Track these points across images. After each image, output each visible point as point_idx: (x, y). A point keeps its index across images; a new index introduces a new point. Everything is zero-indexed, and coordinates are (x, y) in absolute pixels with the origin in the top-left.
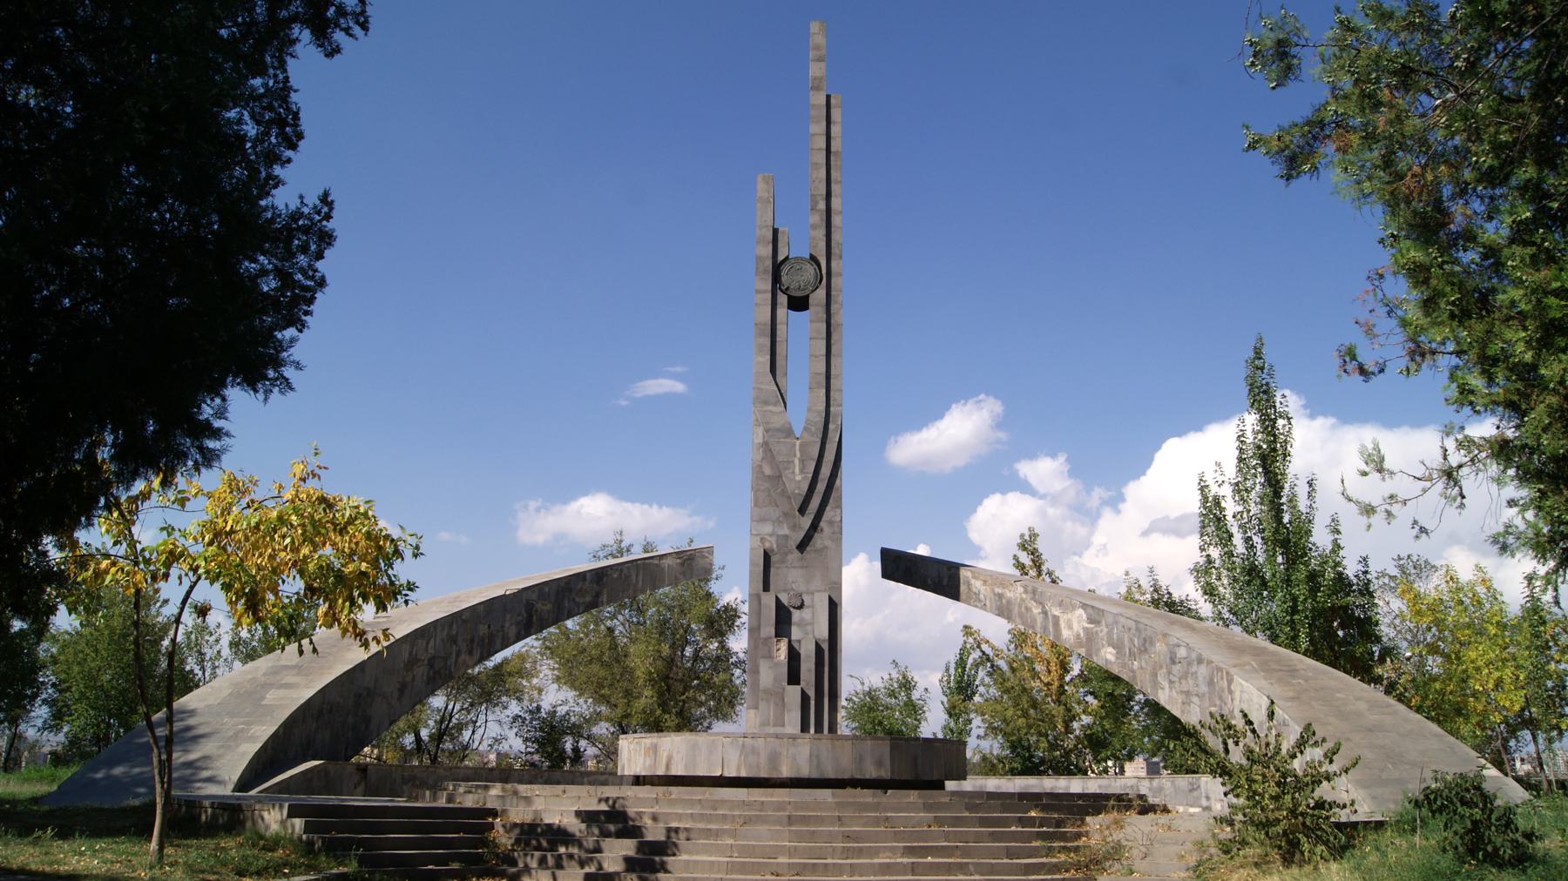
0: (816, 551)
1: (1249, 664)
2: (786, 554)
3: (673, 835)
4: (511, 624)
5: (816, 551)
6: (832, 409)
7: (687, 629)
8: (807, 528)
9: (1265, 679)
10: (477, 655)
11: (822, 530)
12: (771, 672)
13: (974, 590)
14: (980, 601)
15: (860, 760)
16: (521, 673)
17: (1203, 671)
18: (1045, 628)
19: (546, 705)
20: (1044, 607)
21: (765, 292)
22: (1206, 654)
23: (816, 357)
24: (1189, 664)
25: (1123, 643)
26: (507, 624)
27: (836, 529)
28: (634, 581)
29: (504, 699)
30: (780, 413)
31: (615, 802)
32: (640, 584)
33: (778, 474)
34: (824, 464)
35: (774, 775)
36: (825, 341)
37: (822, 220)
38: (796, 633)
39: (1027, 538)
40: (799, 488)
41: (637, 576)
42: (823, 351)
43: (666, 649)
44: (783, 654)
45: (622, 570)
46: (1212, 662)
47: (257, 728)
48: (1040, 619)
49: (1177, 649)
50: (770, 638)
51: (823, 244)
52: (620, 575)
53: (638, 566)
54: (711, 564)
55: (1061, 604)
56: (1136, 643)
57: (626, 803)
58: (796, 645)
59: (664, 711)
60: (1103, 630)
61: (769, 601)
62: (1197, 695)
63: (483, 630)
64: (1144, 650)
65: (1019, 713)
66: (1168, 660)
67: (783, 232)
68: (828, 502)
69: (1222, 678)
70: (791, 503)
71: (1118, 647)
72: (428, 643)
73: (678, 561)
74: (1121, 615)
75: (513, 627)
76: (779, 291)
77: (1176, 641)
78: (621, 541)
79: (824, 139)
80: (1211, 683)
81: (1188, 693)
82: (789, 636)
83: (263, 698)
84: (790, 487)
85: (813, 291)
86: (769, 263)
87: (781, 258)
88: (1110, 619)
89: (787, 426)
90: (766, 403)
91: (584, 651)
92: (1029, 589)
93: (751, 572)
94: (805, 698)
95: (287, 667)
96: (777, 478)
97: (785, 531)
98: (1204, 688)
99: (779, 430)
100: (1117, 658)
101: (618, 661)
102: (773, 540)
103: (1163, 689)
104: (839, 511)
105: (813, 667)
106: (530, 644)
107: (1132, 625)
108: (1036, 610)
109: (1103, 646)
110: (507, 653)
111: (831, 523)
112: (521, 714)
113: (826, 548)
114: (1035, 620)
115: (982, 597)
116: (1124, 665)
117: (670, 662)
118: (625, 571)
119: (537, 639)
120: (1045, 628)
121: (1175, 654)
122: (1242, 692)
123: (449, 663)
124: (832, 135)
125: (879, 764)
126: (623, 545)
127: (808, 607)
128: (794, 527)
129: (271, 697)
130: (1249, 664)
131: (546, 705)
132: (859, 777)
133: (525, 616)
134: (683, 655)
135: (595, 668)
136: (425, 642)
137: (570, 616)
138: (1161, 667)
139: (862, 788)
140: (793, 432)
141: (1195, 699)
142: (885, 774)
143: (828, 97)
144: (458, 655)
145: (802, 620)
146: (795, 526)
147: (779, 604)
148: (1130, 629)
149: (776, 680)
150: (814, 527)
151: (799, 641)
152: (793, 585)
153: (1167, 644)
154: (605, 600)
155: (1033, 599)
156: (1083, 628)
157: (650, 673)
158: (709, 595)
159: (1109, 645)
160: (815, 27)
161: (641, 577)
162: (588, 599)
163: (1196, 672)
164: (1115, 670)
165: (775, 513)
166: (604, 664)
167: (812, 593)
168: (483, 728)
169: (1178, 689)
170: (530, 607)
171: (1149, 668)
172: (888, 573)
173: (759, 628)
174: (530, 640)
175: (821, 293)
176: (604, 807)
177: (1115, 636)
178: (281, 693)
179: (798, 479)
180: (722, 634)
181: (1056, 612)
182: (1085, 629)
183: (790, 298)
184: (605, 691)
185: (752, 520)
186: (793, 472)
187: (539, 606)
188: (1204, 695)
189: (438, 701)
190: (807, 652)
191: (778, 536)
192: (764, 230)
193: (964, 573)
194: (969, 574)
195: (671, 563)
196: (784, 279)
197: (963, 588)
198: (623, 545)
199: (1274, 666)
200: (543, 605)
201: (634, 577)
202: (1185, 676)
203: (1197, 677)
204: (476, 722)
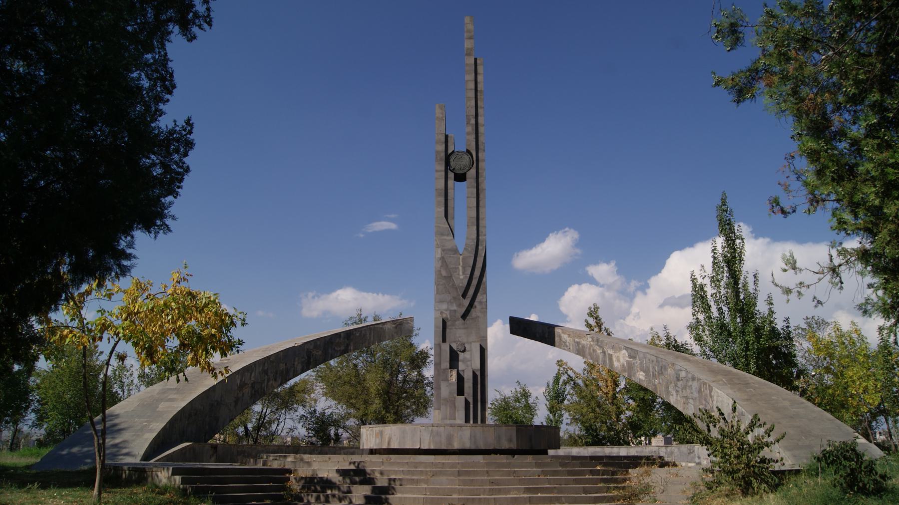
1: (722, 380)
2: (455, 321)
3: (392, 482)
6: (480, 238)
7: (399, 365)
9: (731, 389)
10: (279, 381)
11: (475, 307)
12: (448, 388)
13: (563, 340)
14: (567, 346)
17: (695, 384)
18: (604, 361)
19: (319, 409)
21: (441, 171)
22: (697, 375)
24: (687, 381)
25: (649, 369)
26: (296, 363)
27: (484, 307)
29: (295, 406)
30: (451, 240)
31: (359, 464)
32: (372, 339)
34: (476, 269)
35: (450, 448)
36: (476, 199)
38: (461, 366)
39: (593, 309)
40: (462, 283)
43: (387, 376)
45: (361, 331)
48: (601, 356)
49: (680, 372)
50: (447, 369)
51: (474, 144)
52: (360, 334)
53: (370, 329)
54: (413, 327)
55: (613, 347)
56: (657, 369)
57: (365, 465)
59: (387, 412)
60: (637, 362)
61: (446, 348)
62: (692, 399)
63: (282, 366)
65: (590, 410)
66: (675, 379)
67: (451, 137)
69: (706, 389)
71: (646, 371)
73: (394, 326)
74: (647, 353)
75: (300, 365)
77: (679, 368)
80: (700, 391)
81: (686, 398)
82: (457, 367)
83: (158, 407)
84: (457, 282)
85: (468, 170)
86: (443, 154)
87: (450, 151)
88: (641, 355)
90: (442, 234)
91: (340, 378)
94: (467, 403)
95: (171, 389)
96: (449, 278)
97: (454, 307)
98: (696, 395)
99: (450, 250)
100: (646, 378)
101: (360, 384)
102: (448, 313)
103: (672, 395)
104: (485, 296)
105: (471, 385)
107: (654, 359)
108: (599, 351)
109: (638, 371)
110: (297, 379)
111: (481, 303)
113: (478, 317)
114: (599, 357)
115: (567, 343)
116: (650, 382)
117: (390, 384)
118: (363, 332)
119: (313, 371)
120: (604, 361)
121: (679, 375)
122: (718, 396)
123: (263, 385)
124: (478, 81)
125: (510, 440)
127: (469, 351)
128: (460, 305)
129: (162, 406)
130: (722, 380)
131: (319, 409)
133: (306, 358)
134: (397, 380)
136: (249, 374)
137: (332, 358)
138: (671, 383)
141: (691, 401)
142: (513, 446)
143: (476, 60)
146: (460, 305)
148: (653, 361)
149: (450, 393)
150: (471, 305)
151: (463, 371)
152: (459, 339)
154: (352, 348)
155: (597, 345)
158: (411, 345)
159: (641, 371)
160: (467, 20)
162: (342, 348)
163: (691, 386)
164: (645, 385)
166: (352, 385)
168: (283, 423)
169: (681, 395)
170: (309, 354)
171: (664, 383)
172: (513, 331)
173: (440, 364)
174: (308, 372)
175: (473, 172)
176: (352, 467)
178: (167, 404)
179: (461, 278)
181: (611, 352)
182: (626, 361)
183: (455, 174)
184: (353, 401)
185: (436, 302)
186: (459, 274)
187: (314, 352)
188: (696, 398)
189: (257, 408)
190: (468, 377)
191: (451, 311)
193: (557, 330)
194: (560, 331)
195: (389, 327)
196: (452, 163)
197: (557, 339)
199: (736, 381)
201: (368, 335)
202: (685, 387)
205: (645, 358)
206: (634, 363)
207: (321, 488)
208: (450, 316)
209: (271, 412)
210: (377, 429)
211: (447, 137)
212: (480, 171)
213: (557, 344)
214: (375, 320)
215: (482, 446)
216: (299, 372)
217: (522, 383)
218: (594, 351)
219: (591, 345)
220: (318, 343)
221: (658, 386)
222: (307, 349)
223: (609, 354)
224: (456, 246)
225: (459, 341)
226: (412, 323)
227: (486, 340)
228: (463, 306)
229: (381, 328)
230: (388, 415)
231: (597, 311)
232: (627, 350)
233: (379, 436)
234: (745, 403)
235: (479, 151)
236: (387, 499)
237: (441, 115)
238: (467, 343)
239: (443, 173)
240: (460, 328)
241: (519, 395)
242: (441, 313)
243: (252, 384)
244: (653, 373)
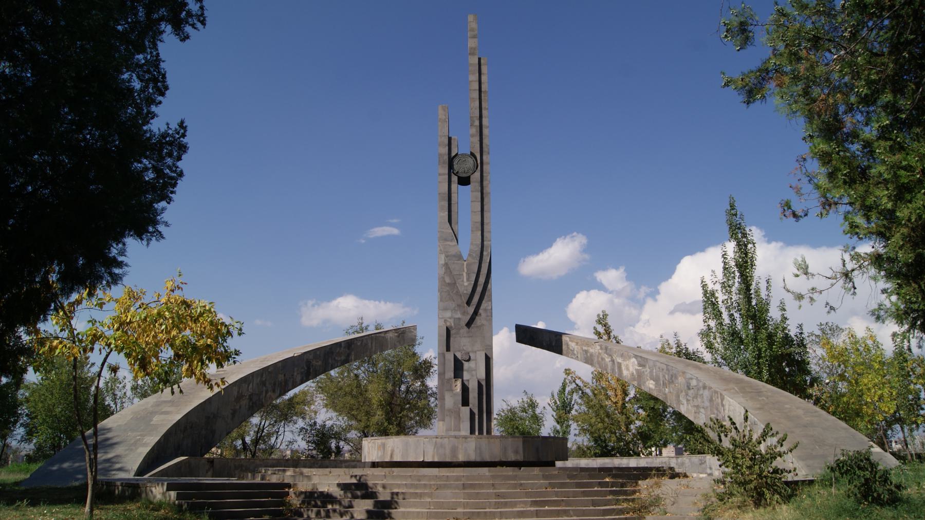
0: (477, 327)
1: (734, 389)
2: (460, 329)
3: (395, 496)
5: (477, 327)
6: (485, 243)
7: (402, 375)
9: (743, 397)
10: (278, 392)
12: (452, 399)
14: (574, 354)
15: (505, 450)
16: (304, 403)
18: (613, 370)
23: (475, 212)
24: (698, 389)
25: (659, 378)
26: (295, 374)
27: (489, 314)
28: (370, 347)
29: (295, 418)
30: (454, 246)
33: (454, 282)
35: (455, 460)
36: (480, 203)
38: (466, 376)
39: (601, 316)
41: (372, 344)
43: (390, 387)
44: (458, 388)
45: (362, 341)
46: (711, 388)
47: (148, 438)
48: (610, 364)
49: (691, 381)
51: (478, 146)
53: (372, 338)
54: (416, 336)
55: (622, 356)
58: (466, 383)
61: (450, 357)
62: (703, 408)
63: (281, 377)
64: (671, 382)
66: (686, 388)
67: (455, 139)
68: (484, 298)
69: (718, 398)
71: (656, 380)
72: (248, 387)
73: (396, 334)
77: (690, 376)
78: (362, 323)
79: (478, 83)
80: (711, 400)
81: (698, 407)
82: (462, 377)
84: (461, 289)
86: (446, 157)
87: (453, 154)
88: (651, 364)
90: (446, 240)
93: (439, 341)
94: (472, 414)
96: (453, 285)
97: (459, 315)
98: (707, 404)
99: (454, 256)
100: (656, 387)
101: (361, 394)
102: (452, 321)
103: (683, 404)
104: (490, 303)
105: (476, 395)
106: (309, 385)
107: (665, 367)
108: (608, 360)
109: (648, 380)
111: (485, 310)
113: (483, 325)
114: (607, 365)
115: (575, 352)
116: (660, 391)
117: (393, 394)
119: (313, 382)
120: (613, 370)
121: (690, 384)
123: (261, 398)
125: (516, 452)
126: (363, 325)
127: (473, 360)
128: (464, 313)
129: (156, 419)
133: (306, 368)
134: (400, 390)
137: (333, 368)
138: (682, 392)
141: (702, 410)
142: (520, 458)
143: (480, 59)
144: (267, 392)
146: (464, 312)
148: (663, 369)
149: (455, 403)
150: (476, 313)
151: (468, 380)
153: (685, 378)
155: (606, 353)
158: (414, 354)
159: (651, 379)
160: (471, 18)
162: (343, 358)
163: (702, 394)
164: (655, 394)
165: (453, 305)
166: (353, 396)
167: (476, 352)
168: (282, 435)
169: (692, 405)
170: (309, 363)
171: (675, 392)
172: (520, 339)
173: (444, 373)
174: (308, 383)
175: (477, 175)
176: (354, 481)
178: (162, 417)
179: (466, 285)
180: (423, 377)
181: (620, 360)
184: (354, 412)
185: (439, 310)
186: (463, 281)
187: (314, 362)
188: (707, 407)
189: (255, 420)
191: (455, 319)
192: (443, 138)
193: (565, 338)
194: (568, 339)
195: (391, 335)
196: (455, 167)
197: (564, 347)
198: (363, 325)
201: (370, 344)
202: (696, 397)
203: (703, 397)
204: (278, 432)
206: (643, 372)
207: (321, 503)
208: (454, 324)
209: (270, 424)
213: (564, 352)
215: (487, 458)
217: (530, 393)
218: (603, 359)
219: (599, 354)
220: (318, 353)
223: (618, 363)
224: (460, 252)
226: (415, 332)
227: (492, 349)
228: (468, 313)
230: (391, 426)
232: (636, 359)
234: (758, 412)
237: (444, 117)
242: (445, 321)
243: (250, 396)
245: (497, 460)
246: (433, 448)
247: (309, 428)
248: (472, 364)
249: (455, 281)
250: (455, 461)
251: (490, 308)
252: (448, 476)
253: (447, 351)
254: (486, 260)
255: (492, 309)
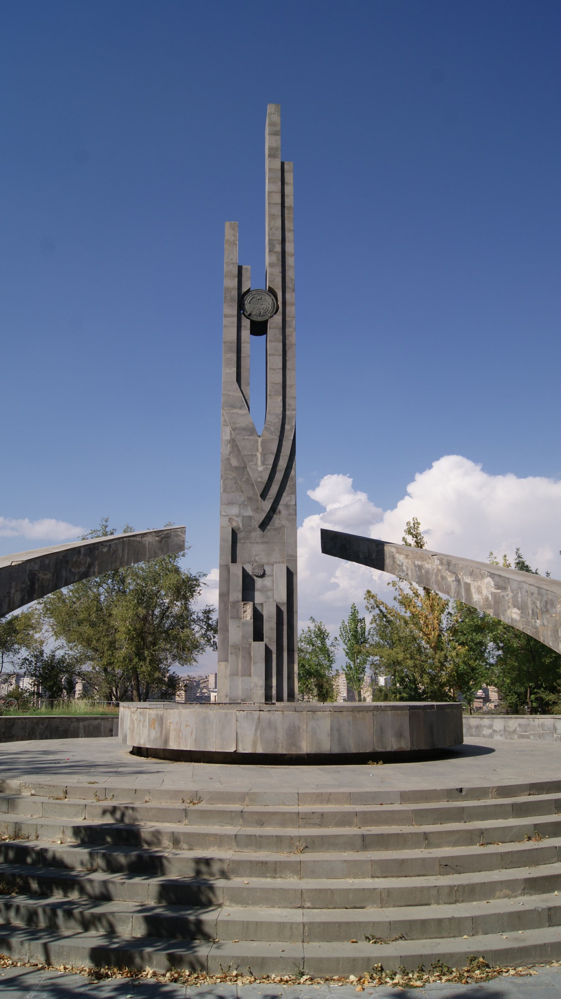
0: (275, 529)
2: (250, 532)
3: (204, 868)
4: (17, 591)
5: (275, 529)
6: (287, 413)
8: (268, 510)
11: (280, 512)
13: (398, 562)
14: (403, 571)
15: (381, 732)
18: (458, 593)
19: (47, 651)
20: (457, 576)
21: (232, 316)
23: (274, 370)
26: (13, 591)
28: (121, 555)
29: (16, 646)
30: (245, 415)
31: (123, 815)
32: (126, 557)
33: (243, 465)
34: (281, 458)
35: (294, 751)
36: (281, 358)
37: (278, 260)
38: (259, 597)
39: (412, 525)
40: (261, 477)
41: (123, 551)
42: (280, 365)
44: (248, 615)
45: (110, 546)
48: (453, 585)
50: (238, 602)
51: (279, 279)
52: (109, 550)
53: (124, 542)
54: (184, 541)
55: (471, 574)
57: (139, 816)
58: (259, 608)
60: (509, 594)
61: (236, 571)
67: (247, 269)
68: (285, 489)
70: (254, 490)
71: (522, 608)
73: (157, 539)
74: (524, 582)
76: (243, 316)
78: (106, 527)
82: (253, 600)
84: (253, 476)
85: (271, 317)
86: (235, 293)
87: (244, 290)
88: (515, 585)
89: (251, 426)
90: (233, 406)
92: (445, 561)
94: (268, 651)
96: (242, 469)
97: (249, 512)
99: (244, 429)
100: (522, 617)
102: (239, 520)
104: (293, 496)
105: (274, 626)
107: (535, 590)
108: (451, 579)
109: (509, 608)
110: (17, 612)
111: (287, 506)
112: (28, 658)
113: (283, 527)
114: (450, 586)
115: (404, 568)
116: (528, 623)
117: (145, 619)
118: (113, 547)
120: (458, 593)
124: (286, 193)
125: (399, 735)
126: (108, 529)
127: (269, 576)
128: (257, 509)
131: (47, 651)
132: (380, 750)
133: (28, 583)
134: (153, 614)
135: (366, 984)
137: (66, 584)
139: (385, 762)
140: (256, 431)
142: (405, 745)
143: (283, 164)
145: (264, 586)
146: (258, 508)
147: (245, 574)
148: (532, 594)
149: (243, 637)
150: (273, 509)
151: (262, 604)
154: (96, 570)
155: (448, 569)
156: (492, 593)
157: (129, 630)
159: (514, 607)
160: (271, 108)
161: (126, 551)
162: (82, 569)
164: (520, 627)
166: (93, 625)
167: (273, 565)
170: (33, 577)
171: (551, 626)
172: (326, 549)
174: (33, 604)
175: (278, 318)
176: (108, 820)
177: (519, 599)
180: (186, 599)
181: (468, 580)
182: (492, 593)
183: (253, 323)
185: (222, 504)
186: (256, 464)
187: (41, 575)
191: (243, 517)
193: (387, 549)
194: (394, 550)
195: (151, 540)
196: (247, 307)
197: (388, 561)
198: (108, 529)
200: (44, 574)
205: (520, 588)
206: (503, 597)
207: (39, 884)
208: (243, 525)
210: (151, 711)
211: (240, 268)
212: (287, 319)
214: (125, 532)
215: (353, 748)
216: (17, 604)
217: (318, 620)
218: (443, 578)
219: (439, 570)
220: (47, 561)
221: (540, 629)
222: (31, 571)
223: (466, 584)
225: (256, 561)
227: (295, 561)
228: (262, 510)
229: (139, 541)
230: (141, 663)
231: (418, 527)
232: (492, 578)
233: (157, 725)
235: (287, 291)
236: (199, 923)
237: (233, 238)
238: (268, 564)
239: (235, 319)
240: (257, 543)
241: (313, 635)
242: (230, 520)
244: (533, 610)
245: (368, 751)
246: (254, 728)
247: (33, 659)
248: (267, 582)
249: (244, 462)
250: (294, 752)
251: (293, 503)
252: (322, 814)
253: (232, 562)
254: (289, 437)
255: (296, 505)
